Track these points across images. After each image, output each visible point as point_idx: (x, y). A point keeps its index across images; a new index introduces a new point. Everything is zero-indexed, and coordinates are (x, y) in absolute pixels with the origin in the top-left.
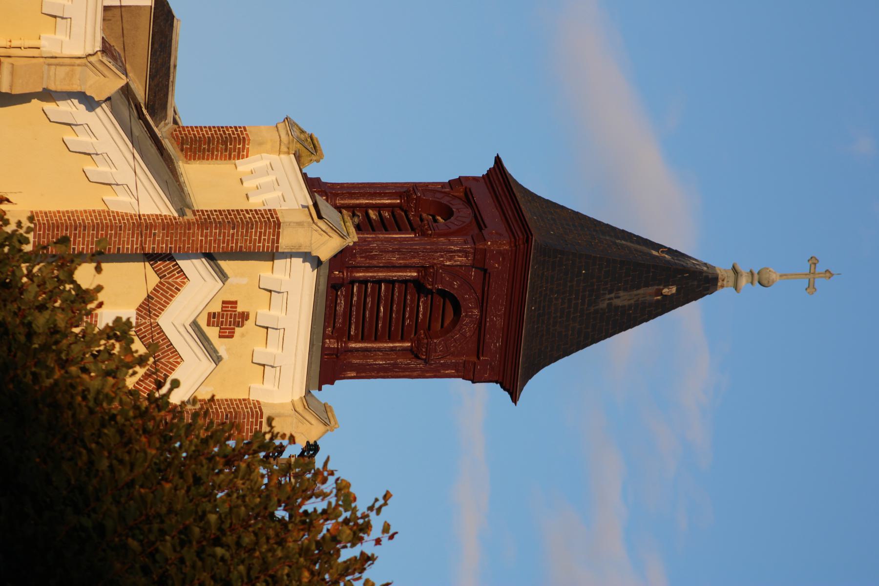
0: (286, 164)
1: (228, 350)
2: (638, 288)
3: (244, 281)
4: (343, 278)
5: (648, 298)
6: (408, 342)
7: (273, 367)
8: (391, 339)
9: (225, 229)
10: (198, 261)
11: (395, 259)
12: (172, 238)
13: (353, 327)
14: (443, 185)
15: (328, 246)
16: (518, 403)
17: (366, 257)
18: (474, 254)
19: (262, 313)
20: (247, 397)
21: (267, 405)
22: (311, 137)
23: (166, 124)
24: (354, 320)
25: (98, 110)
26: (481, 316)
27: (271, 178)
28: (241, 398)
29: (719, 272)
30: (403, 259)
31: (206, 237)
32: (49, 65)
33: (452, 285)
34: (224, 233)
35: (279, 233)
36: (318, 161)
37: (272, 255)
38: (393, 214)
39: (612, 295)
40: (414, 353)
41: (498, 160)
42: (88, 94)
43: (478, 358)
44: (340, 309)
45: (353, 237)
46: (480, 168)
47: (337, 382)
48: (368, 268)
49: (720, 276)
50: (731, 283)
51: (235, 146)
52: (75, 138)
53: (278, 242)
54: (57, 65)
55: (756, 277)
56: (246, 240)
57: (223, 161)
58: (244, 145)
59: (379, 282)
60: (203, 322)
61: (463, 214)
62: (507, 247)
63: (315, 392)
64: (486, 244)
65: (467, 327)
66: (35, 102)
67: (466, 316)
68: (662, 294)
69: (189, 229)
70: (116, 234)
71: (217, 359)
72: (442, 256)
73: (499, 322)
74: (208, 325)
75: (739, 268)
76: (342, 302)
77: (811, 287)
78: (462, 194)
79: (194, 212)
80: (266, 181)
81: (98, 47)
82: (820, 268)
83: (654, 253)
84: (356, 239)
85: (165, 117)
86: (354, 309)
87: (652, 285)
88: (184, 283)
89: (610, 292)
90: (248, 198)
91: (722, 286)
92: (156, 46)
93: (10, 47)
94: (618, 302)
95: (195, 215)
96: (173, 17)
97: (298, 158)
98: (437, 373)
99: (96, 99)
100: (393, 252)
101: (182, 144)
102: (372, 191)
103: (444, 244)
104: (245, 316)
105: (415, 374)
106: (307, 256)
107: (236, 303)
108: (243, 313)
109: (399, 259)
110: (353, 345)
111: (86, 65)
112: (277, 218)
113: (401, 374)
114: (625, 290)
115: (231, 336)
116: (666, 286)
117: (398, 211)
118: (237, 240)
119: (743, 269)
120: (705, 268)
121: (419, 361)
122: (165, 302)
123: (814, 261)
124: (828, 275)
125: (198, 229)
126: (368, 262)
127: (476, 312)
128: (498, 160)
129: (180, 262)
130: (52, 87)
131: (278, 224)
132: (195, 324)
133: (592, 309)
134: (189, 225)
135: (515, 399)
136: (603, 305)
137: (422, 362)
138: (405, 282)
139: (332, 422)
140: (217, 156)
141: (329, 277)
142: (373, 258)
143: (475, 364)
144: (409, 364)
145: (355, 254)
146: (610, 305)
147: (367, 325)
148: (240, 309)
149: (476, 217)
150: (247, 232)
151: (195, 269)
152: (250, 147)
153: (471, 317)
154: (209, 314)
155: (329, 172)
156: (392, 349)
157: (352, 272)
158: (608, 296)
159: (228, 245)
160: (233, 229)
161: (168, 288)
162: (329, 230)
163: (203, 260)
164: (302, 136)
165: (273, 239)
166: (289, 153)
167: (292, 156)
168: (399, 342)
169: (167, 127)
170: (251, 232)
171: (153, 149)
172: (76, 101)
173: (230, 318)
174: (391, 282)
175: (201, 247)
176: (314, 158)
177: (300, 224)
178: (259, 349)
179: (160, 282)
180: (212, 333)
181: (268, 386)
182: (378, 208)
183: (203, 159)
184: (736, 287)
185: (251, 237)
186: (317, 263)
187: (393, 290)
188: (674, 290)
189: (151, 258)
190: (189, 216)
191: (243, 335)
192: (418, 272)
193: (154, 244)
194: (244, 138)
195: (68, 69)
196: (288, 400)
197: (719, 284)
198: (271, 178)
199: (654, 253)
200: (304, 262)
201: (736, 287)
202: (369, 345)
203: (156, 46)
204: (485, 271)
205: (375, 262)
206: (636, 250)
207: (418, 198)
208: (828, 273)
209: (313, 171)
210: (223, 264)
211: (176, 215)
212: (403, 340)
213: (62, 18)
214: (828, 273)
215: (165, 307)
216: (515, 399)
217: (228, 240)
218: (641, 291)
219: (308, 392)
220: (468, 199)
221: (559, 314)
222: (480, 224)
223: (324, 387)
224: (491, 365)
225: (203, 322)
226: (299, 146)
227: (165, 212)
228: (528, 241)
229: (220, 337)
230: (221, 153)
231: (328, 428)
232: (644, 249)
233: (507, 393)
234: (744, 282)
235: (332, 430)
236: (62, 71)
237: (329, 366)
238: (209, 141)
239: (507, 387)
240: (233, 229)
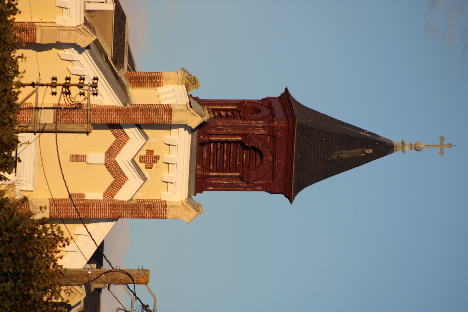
1: (150, 175)
2: (353, 149)
3: (157, 140)
4: (205, 140)
5: (358, 155)
6: (238, 173)
7: (172, 183)
11: (230, 131)
12: (120, 116)
13: (211, 165)
14: (259, 101)
16: (293, 203)
17: (216, 129)
18: (269, 128)
19: (166, 156)
20: (159, 199)
21: (168, 202)
22: (194, 78)
23: (123, 71)
24: (211, 162)
25: (84, 53)
26: (273, 159)
27: (172, 94)
28: (157, 199)
29: (394, 143)
30: (234, 131)
31: (136, 116)
32: (59, 30)
33: (258, 144)
34: (145, 114)
35: (171, 114)
36: (197, 88)
37: (169, 127)
39: (339, 152)
40: (241, 178)
41: (286, 89)
42: (78, 44)
43: (273, 181)
44: (205, 155)
46: (277, 93)
47: (204, 192)
48: (217, 135)
49: (395, 145)
50: (401, 149)
51: (156, 80)
52: (74, 68)
53: (171, 119)
54: (63, 30)
55: (413, 146)
56: (156, 118)
59: (223, 142)
60: (137, 160)
61: (265, 112)
62: (284, 125)
63: (193, 197)
64: (274, 124)
65: (267, 165)
66: (54, 50)
67: (266, 160)
68: (365, 153)
69: (128, 112)
70: (93, 114)
71: (145, 179)
72: (253, 130)
73: (282, 163)
74: (140, 162)
75: (405, 141)
77: (442, 152)
78: (267, 105)
79: (131, 105)
80: (171, 94)
81: (82, 22)
82: (445, 142)
83: (361, 133)
85: (123, 67)
86: (211, 156)
87: (359, 148)
88: (128, 140)
89: (338, 150)
91: (396, 151)
92: (116, 30)
93: (42, 22)
94: (342, 156)
96: (125, 17)
97: (187, 87)
98: (253, 188)
99: (82, 47)
100: (229, 127)
101: (131, 79)
103: (254, 123)
104: (157, 158)
105: (242, 189)
106: (186, 127)
107: (153, 151)
108: (157, 156)
109: (232, 131)
110: (211, 174)
111: (76, 30)
112: (171, 108)
113: (235, 189)
114: (346, 150)
115: (151, 168)
116: (367, 149)
117: (235, 112)
118: (151, 118)
119: (407, 142)
120: (387, 141)
121: (244, 182)
122: (115, 145)
123: (442, 139)
126: (217, 132)
127: (271, 158)
128: (286, 89)
129: (125, 130)
130: (61, 41)
131: (171, 110)
133: (329, 159)
134: (128, 110)
135: (291, 202)
136: (335, 157)
137: (246, 183)
138: (236, 142)
139: (200, 210)
141: (198, 138)
142: (219, 130)
143: (271, 184)
144: (239, 184)
145: (210, 128)
146: (338, 157)
147: (218, 164)
149: (272, 113)
150: (156, 113)
151: (132, 133)
152: (163, 81)
153: (268, 160)
154: (140, 156)
155: (204, 93)
156: (230, 176)
157: (209, 137)
158: (337, 153)
159: (147, 120)
160: (149, 112)
161: (120, 143)
162: (195, 113)
163: (136, 128)
164: (189, 77)
165: (169, 118)
166: (182, 84)
167: (184, 86)
168: (234, 173)
169: (124, 72)
171: (112, 76)
172: (73, 49)
173: (150, 159)
174: (229, 143)
175: (134, 121)
176: (194, 86)
177: (181, 110)
179: (116, 140)
181: (170, 193)
183: (141, 86)
184: (403, 151)
186: (191, 131)
187: (230, 147)
188: (371, 151)
189: (111, 127)
190: (129, 106)
191: (157, 167)
192: (242, 138)
193: (111, 119)
194: (160, 77)
195: (68, 32)
196: (180, 200)
197: (395, 149)
198: (172, 94)
199: (361, 133)
200: (185, 130)
201: (403, 151)
202: (219, 174)
203: (116, 30)
205: (220, 132)
206: (352, 131)
208: (450, 145)
209: (195, 93)
210: (146, 131)
211: (122, 105)
212: (236, 172)
213: (66, 8)
214: (450, 145)
215: (119, 152)
216: (291, 202)
217: (147, 118)
218: (354, 151)
219: (189, 196)
221: (312, 160)
222: (273, 114)
223: (197, 194)
224: (279, 184)
225: (137, 160)
226: (187, 80)
227: (117, 104)
228: (294, 122)
229: (146, 168)
231: (198, 213)
232: (357, 131)
234: (407, 148)
235: (200, 214)
236: (65, 33)
237: (200, 183)
238: (144, 78)
239: (287, 196)
240: (149, 112)
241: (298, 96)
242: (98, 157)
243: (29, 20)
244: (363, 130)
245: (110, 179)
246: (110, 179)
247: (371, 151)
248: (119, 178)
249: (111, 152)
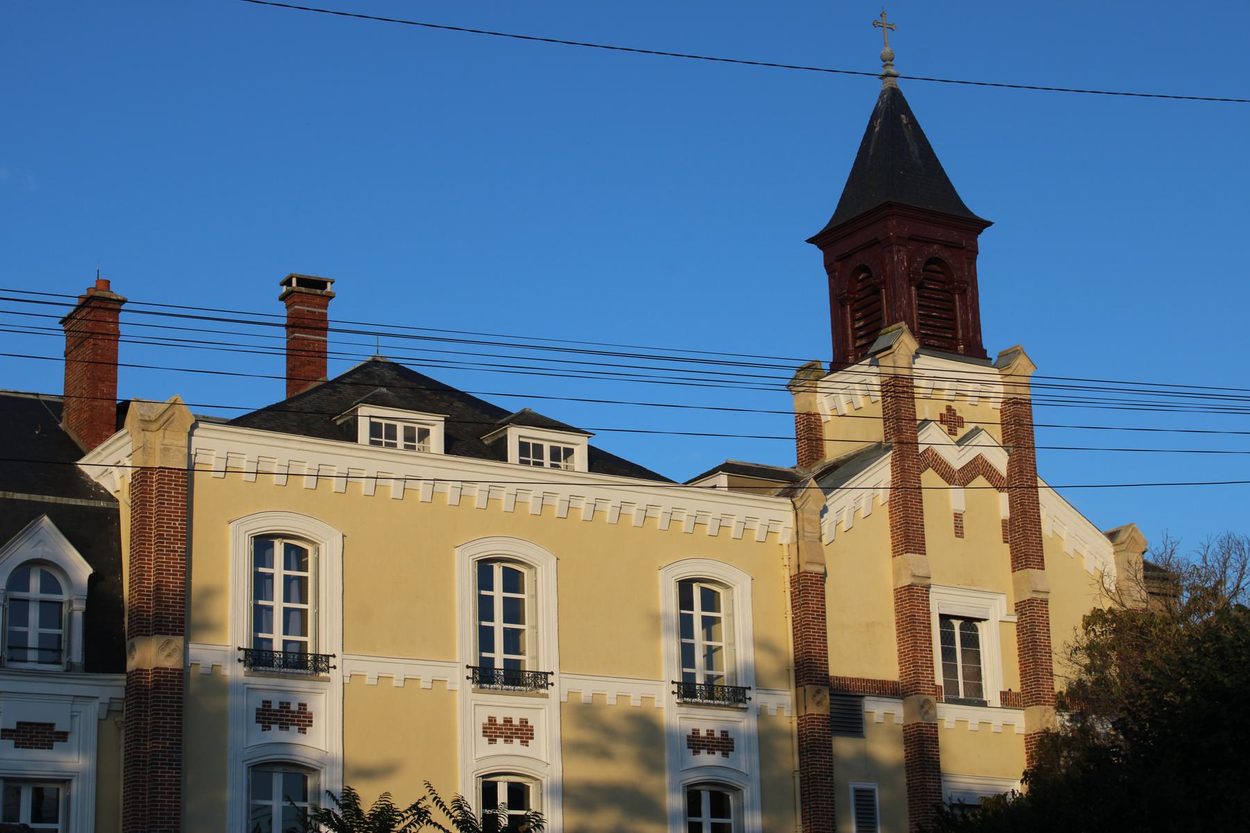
8: (953, 309)
15: (907, 343)
38: (857, 311)
41: (810, 241)
44: (936, 343)
45: (903, 325)
46: (817, 255)
60: (956, 438)
63: (993, 362)
65: (945, 254)
76: (932, 342)
82: (879, 19)
83: (877, 129)
94: (917, 152)
128: (810, 241)
132: (959, 443)
135: (989, 224)
155: (826, 354)
169: (752, 512)
173: (951, 420)
180: (961, 432)
182: (854, 320)
199: (877, 129)
204: (910, 239)
216: (989, 224)
227: (889, 460)
241: (821, 219)
242: (957, 498)
243: (788, 585)
244: (871, 127)
245: (980, 481)
246: (980, 481)
248: (978, 467)
249: (948, 475)
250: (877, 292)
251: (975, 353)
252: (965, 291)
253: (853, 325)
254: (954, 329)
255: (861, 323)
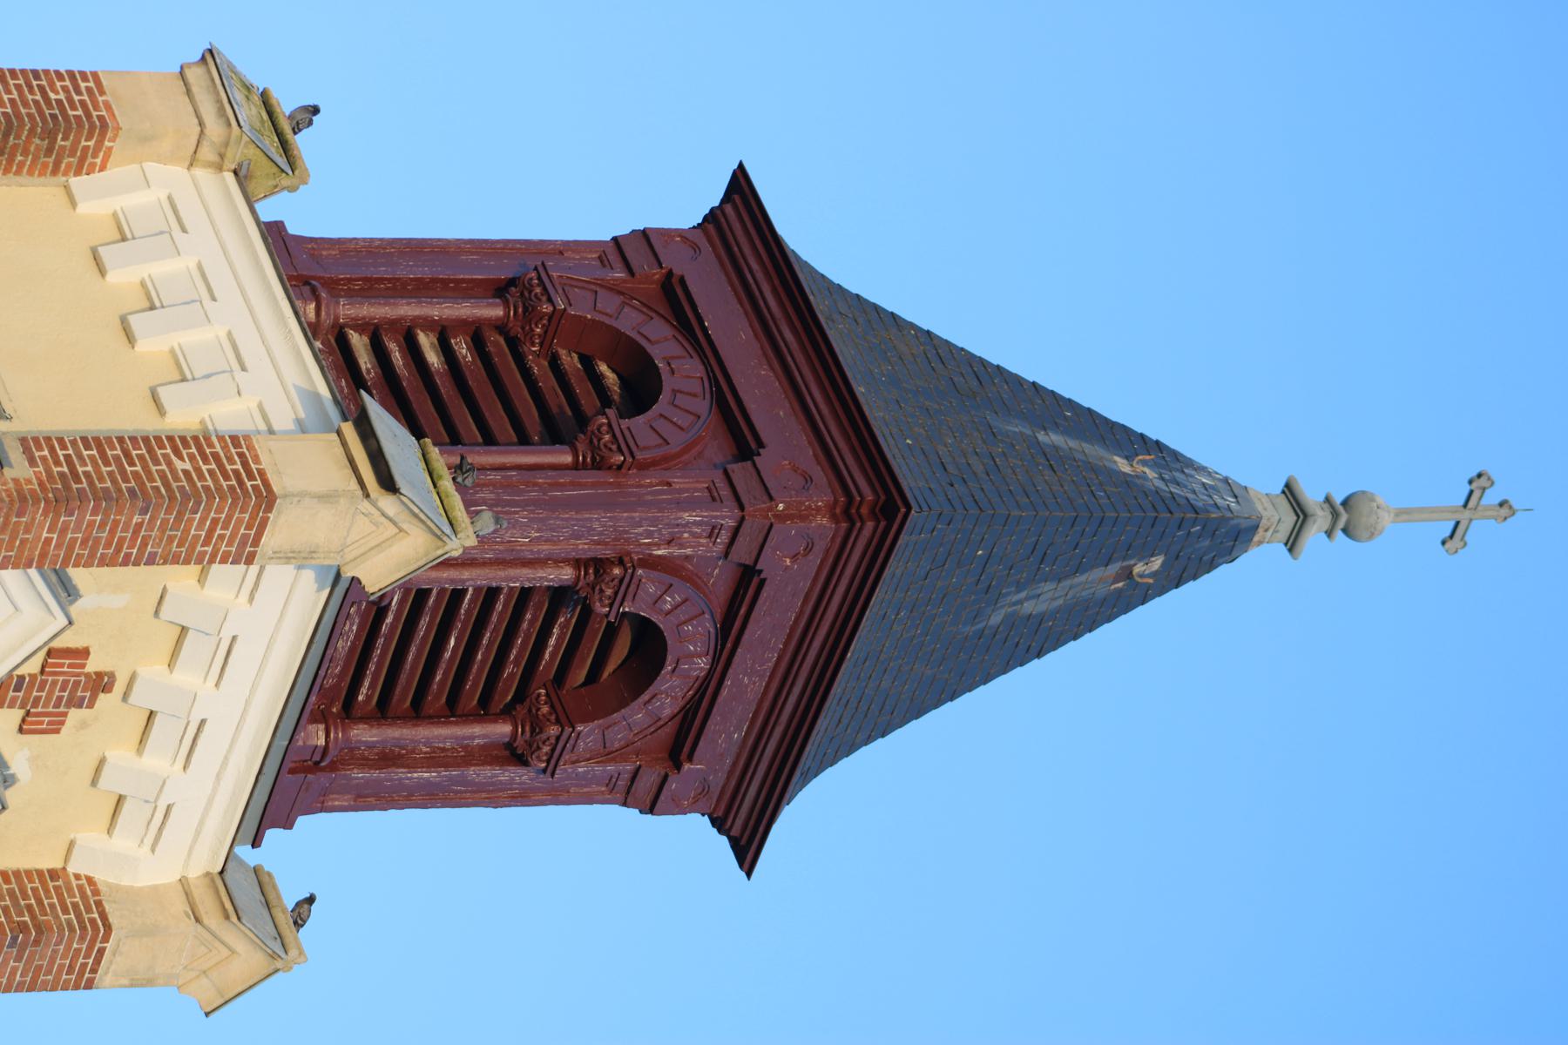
0: (209, 198)
8: (452, 710)
9: (120, 513)
10: (18, 573)
15: (394, 543)
19: (155, 680)
20: (57, 864)
24: (372, 667)
38: (478, 343)
46: (686, 203)
47: (302, 821)
51: (76, 142)
53: (256, 542)
56: (171, 539)
57: (35, 179)
58: (100, 143)
63: (244, 852)
65: (667, 695)
82: (1492, 497)
84: (472, 541)
90: (131, 339)
94: (1028, 607)
95: (32, 462)
102: (425, 272)
104: (101, 683)
107: (84, 653)
108: (100, 675)
119: (1312, 495)
124: (1504, 511)
125: (45, 514)
128: (740, 185)
140: (21, 165)
148: (92, 666)
152: (117, 146)
155: (312, 214)
160: (144, 511)
166: (219, 168)
170: (191, 520)
176: (285, 182)
177: (327, 498)
178: (120, 756)
184: (1292, 544)
185: (187, 531)
191: (83, 725)
197: (1256, 539)
199: (1123, 465)
207: (557, 316)
217: (122, 540)
220: (674, 300)
226: (252, 152)
230: (34, 161)
233: (724, 839)
241: (823, 235)
247: (1157, 563)
250: (554, 435)
251: (296, 782)
252: (521, 760)
253: (428, 324)
254: (383, 711)
255: (433, 358)
